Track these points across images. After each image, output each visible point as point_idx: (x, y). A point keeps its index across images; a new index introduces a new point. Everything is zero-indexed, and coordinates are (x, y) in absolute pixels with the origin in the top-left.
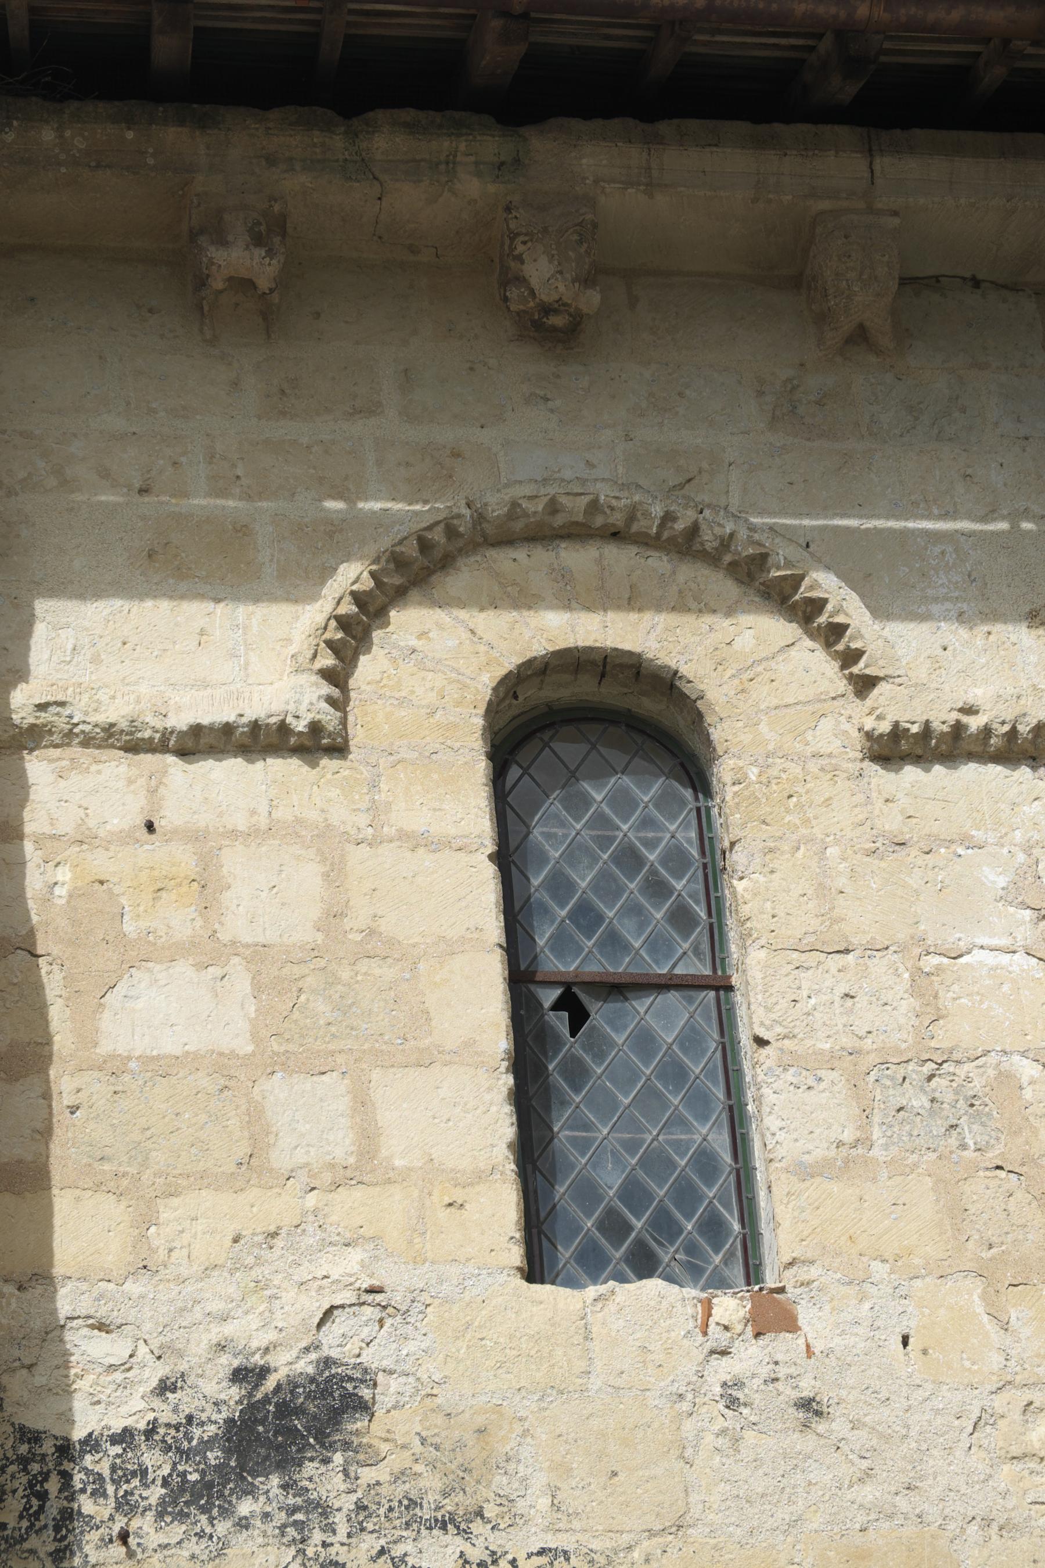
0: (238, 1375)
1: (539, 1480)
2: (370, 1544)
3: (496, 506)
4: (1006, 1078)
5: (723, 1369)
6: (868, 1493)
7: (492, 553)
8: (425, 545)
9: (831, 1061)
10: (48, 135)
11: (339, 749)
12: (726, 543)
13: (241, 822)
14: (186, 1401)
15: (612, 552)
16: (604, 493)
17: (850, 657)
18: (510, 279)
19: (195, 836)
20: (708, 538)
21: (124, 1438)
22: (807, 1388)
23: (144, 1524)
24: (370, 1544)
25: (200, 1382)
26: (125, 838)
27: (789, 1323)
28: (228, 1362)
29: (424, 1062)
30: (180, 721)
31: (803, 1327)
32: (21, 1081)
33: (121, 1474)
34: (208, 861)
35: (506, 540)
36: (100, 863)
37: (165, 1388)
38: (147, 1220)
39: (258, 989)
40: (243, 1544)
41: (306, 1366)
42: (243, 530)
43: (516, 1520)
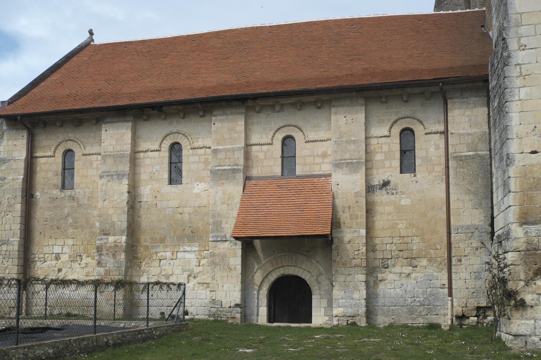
0: (383, 181)
1: (400, 187)
2: (390, 191)
3: (401, 117)
4: (432, 158)
5: (412, 179)
6: (420, 187)
7: (401, 120)
8: (396, 120)
9: (420, 158)
10: (371, 92)
11: (390, 137)
12: (416, 118)
13: (383, 142)
14: (380, 183)
15: (409, 119)
16: (408, 115)
17: (424, 127)
18: (403, 98)
19: (381, 144)
20: (415, 118)
21: (377, 185)
22: (417, 181)
23: (378, 190)
24: (390, 191)
25: (76, 196)
26: (376, 144)
27: (416, 176)
28: (382, 180)
29: (394, 159)
30: (380, 136)
31: (391, 179)
32: (421, 321)
33: (376, 187)
34: (382, 146)
35: (401, 119)
36: (375, 146)
37: (379, 182)
38: (378, 171)
39: (384, 155)
40: (383, 191)
41: (387, 180)
42: (384, 120)
43: (399, 189)
